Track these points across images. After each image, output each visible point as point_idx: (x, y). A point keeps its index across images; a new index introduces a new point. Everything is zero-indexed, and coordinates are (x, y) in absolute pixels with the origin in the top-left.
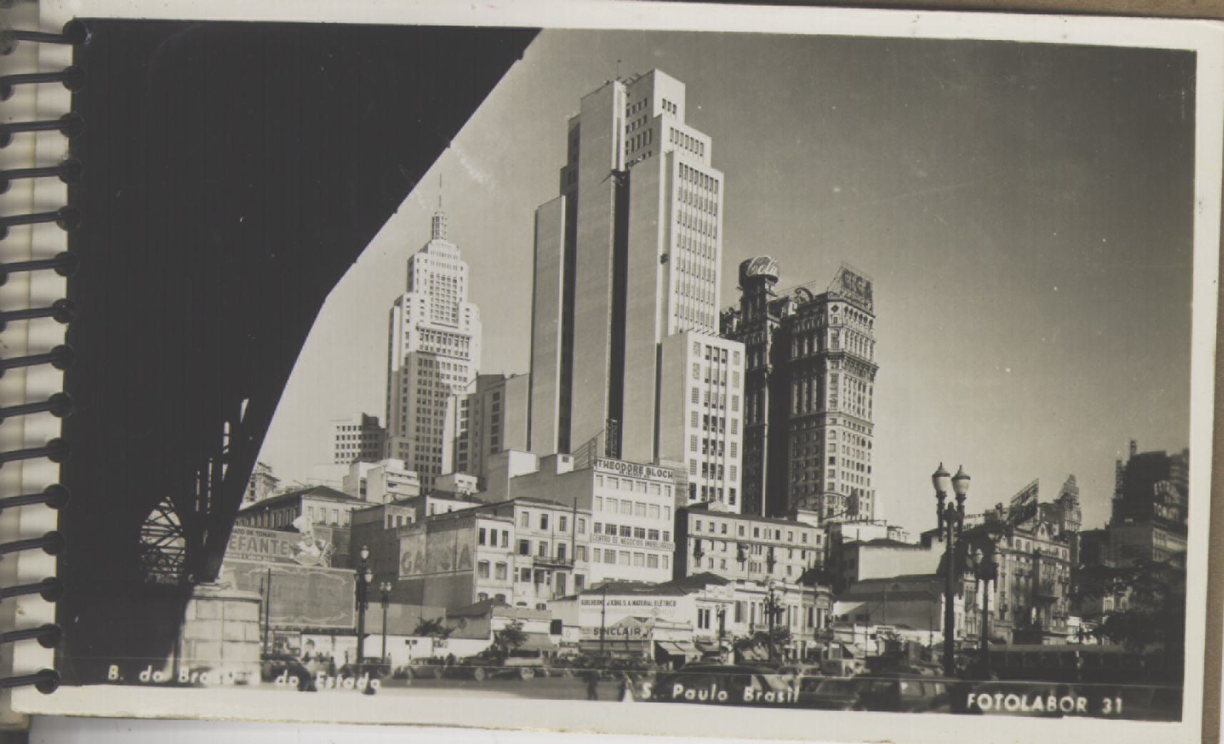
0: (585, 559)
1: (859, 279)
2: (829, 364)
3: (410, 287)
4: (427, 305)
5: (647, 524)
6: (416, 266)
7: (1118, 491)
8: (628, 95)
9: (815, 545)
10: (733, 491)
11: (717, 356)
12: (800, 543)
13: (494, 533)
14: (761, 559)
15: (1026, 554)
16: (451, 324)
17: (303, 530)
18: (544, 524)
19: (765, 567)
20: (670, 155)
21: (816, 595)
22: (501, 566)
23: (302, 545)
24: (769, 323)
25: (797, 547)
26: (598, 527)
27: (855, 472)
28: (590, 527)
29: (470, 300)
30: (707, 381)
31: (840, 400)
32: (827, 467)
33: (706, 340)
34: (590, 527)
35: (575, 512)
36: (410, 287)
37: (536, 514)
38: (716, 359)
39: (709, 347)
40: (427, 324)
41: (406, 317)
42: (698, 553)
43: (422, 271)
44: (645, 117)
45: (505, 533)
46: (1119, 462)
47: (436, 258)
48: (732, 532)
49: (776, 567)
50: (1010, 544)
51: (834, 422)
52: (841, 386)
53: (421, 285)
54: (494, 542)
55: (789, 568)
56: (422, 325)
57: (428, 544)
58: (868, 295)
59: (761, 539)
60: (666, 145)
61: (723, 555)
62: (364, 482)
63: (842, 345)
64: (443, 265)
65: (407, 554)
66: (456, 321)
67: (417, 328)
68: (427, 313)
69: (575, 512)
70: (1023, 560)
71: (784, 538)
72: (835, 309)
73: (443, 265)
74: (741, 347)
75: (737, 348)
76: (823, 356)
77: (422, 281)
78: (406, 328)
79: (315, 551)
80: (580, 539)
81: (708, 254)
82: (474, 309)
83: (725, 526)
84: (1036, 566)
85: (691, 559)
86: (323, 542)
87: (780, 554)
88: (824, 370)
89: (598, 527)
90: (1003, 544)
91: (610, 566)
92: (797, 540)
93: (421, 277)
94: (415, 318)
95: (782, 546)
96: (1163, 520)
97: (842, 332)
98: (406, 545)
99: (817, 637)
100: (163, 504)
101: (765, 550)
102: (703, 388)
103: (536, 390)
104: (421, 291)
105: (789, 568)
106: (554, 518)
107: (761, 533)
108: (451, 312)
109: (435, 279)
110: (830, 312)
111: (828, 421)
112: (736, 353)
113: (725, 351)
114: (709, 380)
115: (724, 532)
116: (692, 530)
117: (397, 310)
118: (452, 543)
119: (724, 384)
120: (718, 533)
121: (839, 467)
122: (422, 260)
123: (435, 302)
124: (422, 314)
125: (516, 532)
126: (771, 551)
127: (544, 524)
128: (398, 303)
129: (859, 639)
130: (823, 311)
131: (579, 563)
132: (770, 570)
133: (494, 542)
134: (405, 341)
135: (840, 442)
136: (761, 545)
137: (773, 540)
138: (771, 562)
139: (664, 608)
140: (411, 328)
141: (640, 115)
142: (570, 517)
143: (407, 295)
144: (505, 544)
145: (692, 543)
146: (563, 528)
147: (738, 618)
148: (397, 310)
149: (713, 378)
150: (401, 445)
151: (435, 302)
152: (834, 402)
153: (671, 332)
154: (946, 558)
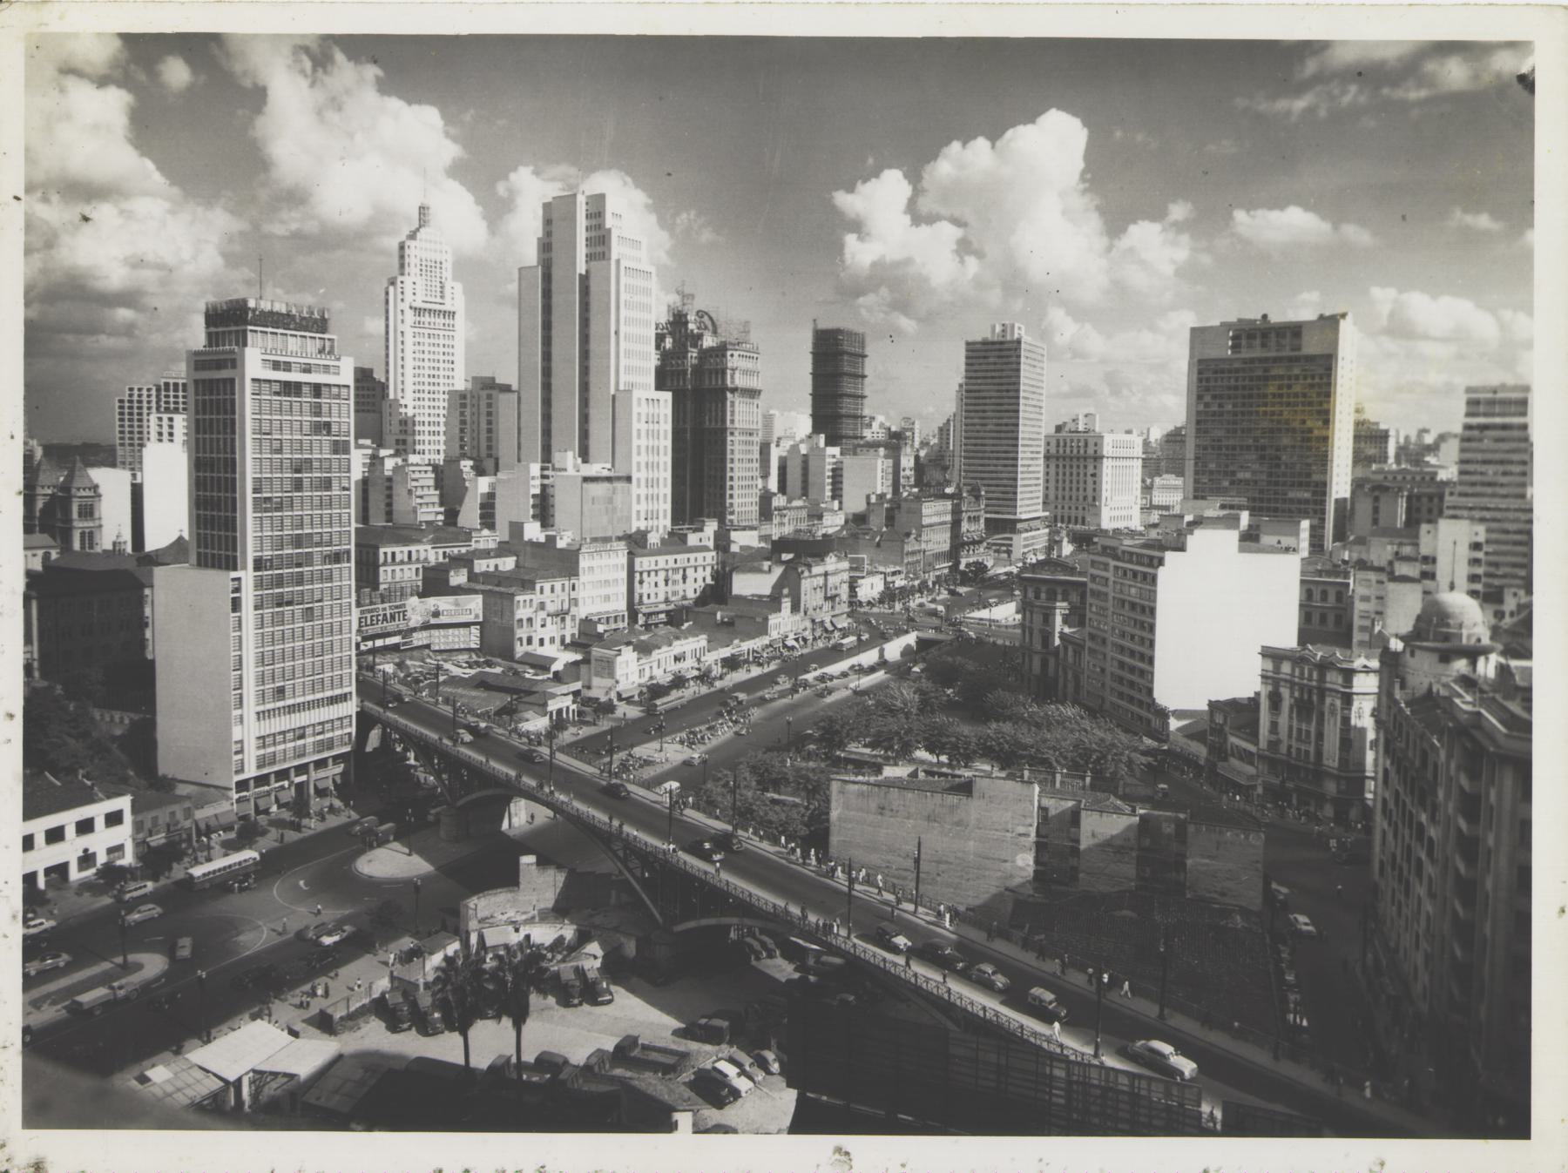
2: (729, 395)
6: (407, 251)
14: (679, 577)
18: (552, 590)
20: (618, 261)
22: (530, 620)
29: (455, 279)
32: (729, 483)
37: (547, 586)
40: (419, 304)
48: (662, 565)
53: (412, 269)
62: (390, 479)
71: (692, 563)
78: (401, 306)
81: (647, 292)
82: (459, 287)
87: (690, 572)
88: (725, 398)
90: (806, 574)
92: (700, 562)
94: (409, 297)
100: (782, 969)
102: (643, 427)
106: (558, 586)
114: (650, 420)
116: (637, 568)
117: (391, 289)
121: (736, 465)
125: (537, 598)
127: (552, 590)
128: (393, 282)
130: (724, 356)
134: (400, 317)
135: (737, 447)
140: (405, 306)
141: (594, 222)
143: (400, 278)
145: (637, 576)
148: (391, 289)
152: (732, 421)
153: (622, 387)
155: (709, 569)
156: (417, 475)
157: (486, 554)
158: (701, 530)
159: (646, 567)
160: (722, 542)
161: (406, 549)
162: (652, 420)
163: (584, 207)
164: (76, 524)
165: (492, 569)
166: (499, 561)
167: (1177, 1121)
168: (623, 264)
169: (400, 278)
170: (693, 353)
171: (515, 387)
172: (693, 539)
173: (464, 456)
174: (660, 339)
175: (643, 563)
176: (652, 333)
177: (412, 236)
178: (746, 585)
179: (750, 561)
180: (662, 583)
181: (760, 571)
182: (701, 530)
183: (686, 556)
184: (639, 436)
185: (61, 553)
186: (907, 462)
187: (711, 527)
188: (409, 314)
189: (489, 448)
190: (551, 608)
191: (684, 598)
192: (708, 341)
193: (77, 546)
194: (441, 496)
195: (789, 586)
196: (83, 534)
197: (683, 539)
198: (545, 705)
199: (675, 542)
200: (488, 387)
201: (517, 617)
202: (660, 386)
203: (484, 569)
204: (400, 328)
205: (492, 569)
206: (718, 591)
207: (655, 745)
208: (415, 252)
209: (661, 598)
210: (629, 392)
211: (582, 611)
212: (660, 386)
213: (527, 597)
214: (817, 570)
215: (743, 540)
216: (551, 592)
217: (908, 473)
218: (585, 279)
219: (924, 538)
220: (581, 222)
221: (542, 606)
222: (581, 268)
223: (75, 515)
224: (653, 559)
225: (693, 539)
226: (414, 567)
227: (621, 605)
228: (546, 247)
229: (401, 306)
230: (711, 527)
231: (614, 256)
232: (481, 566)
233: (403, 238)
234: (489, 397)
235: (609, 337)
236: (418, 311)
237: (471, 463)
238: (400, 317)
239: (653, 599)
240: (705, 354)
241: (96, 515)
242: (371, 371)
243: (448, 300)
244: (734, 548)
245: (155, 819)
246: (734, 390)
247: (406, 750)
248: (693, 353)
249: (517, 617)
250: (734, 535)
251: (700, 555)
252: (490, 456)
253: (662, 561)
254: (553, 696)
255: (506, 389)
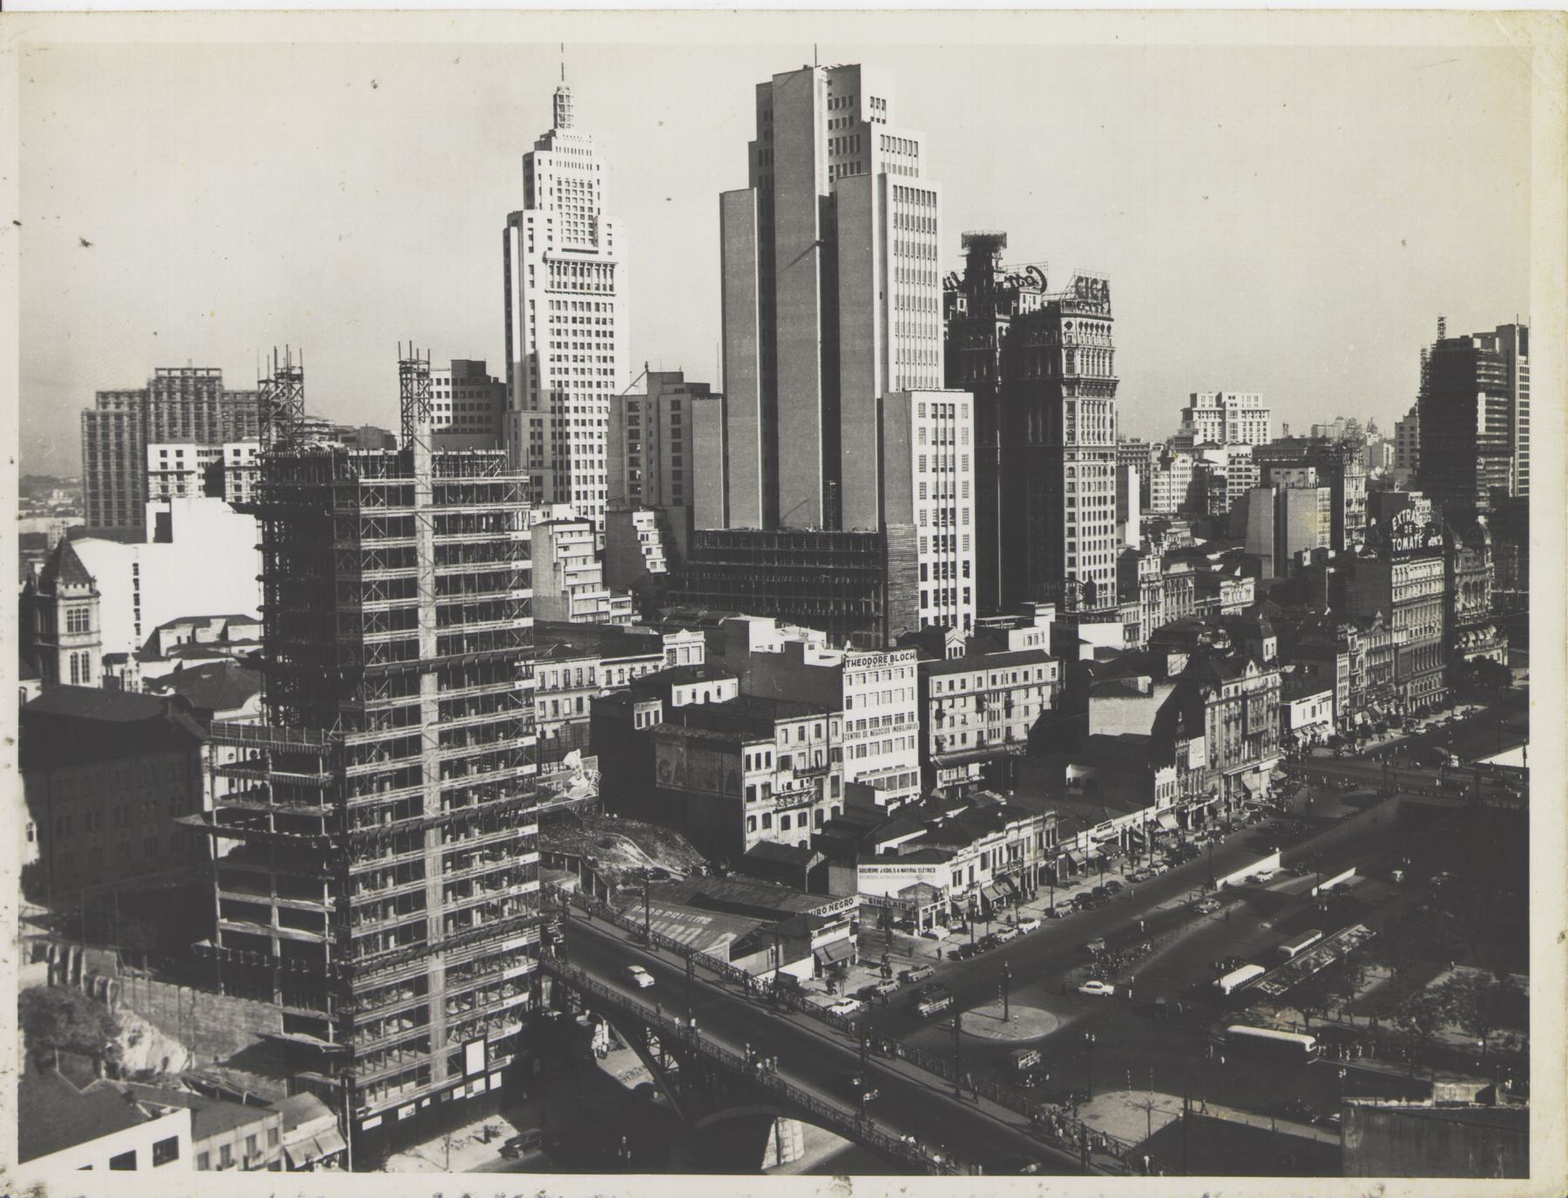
0: (840, 759)
1: (1095, 281)
2: (1064, 392)
3: (530, 204)
4: (555, 225)
5: (892, 710)
6: (537, 169)
7: (1423, 390)
8: (829, 83)
9: (1050, 679)
10: (966, 563)
11: (945, 412)
12: (1036, 681)
13: (758, 756)
14: (998, 706)
15: (1234, 699)
16: (590, 247)
17: (573, 765)
19: (1003, 713)
20: (883, 177)
21: (1044, 821)
23: (573, 780)
24: (998, 324)
25: (1033, 685)
26: (849, 725)
27: (1097, 508)
28: (842, 728)
30: (935, 443)
31: (1079, 431)
33: (930, 398)
34: (842, 728)
35: (828, 718)
36: (530, 204)
37: (793, 729)
38: (943, 416)
39: (935, 405)
40: (557, 254)
41: (527, 243)
42: (940, 715)
43: (545, 177)
44: (851, 118)
45: (768, 755)
46: (1424, 350)
47: (563, 157)
48: (971, 685)
49: (1014, 711)
50: (1219, 695)
51: (1072, 458)
52: (1079, 415)
53: (544, 198)
54: (758, 766)
55: (1027, 708)
56: (550, 255)
57: (689, 758)
58: (1106, 297)
59: (999, 686)
60: (877, 158)
61: (963, 710)
63: (1078, 370)
64: (574, 165)
65: (665, 763)
66: (594, 242)
67: (545, 260)
68: (556, 235)
69: (828, 718)
70: (1232, 705)
71: (1020, 680)
72: (1069, 325)
73: (574, 165)
74: (969, 398)
75: (964, 400)
76: (1058, 380)
77: (546, 191)
79: (584, 783)
80: (835, 741)
83: (963, 681)
84: (1244, 707)
85: (933, 722)
86: (590, 771)
87: (1017, 696)
89: (849, 725)
90: (1213, 698)
91: (862, 759)
92: (1033, 678)
93: (543, 184)
94: (541, 244)
95: (1019, 688)
96: (1404, 553)
97: (1078, 354)
98: (661, 753)
99: (1046, 857)
101: (1002, 696)
102: (930, 451)
103: (731, 421)
104: (546, 206)
105: (1027, 708)
106: (810, 728)
107: (998, 680)
108: (587, 229)
109: (564, 186)
110: (1064, 329)
111: (1066, 457)
112: (965, 406)
113: (953, 405)
115: (963, 687)
116: (934, 693)
118: (717, 765)
119: (952, 443)
120: (958, 689)
122: (545, 162)
123: (566, 218)
124: (550, 238)
125: (776, 750)
126: (1009, 696)
127: (802, 737)
129: (1082, 844)
131: (834, 766)
132: (1008, 715)
133: (758, 766)
136: (998, 691)
137: (1011, 684)
138: (1009, 706)
139: (926, 874)
140: (535, 259)
142: (823, 723)
143: (527, 214)
144: (768, 764)
145: (935, 705)
146: (818, 734)
147: (984, 866)
148: (514, 231)
149: (941, 438)
150: (532, 422)
151: (566, 218)
152: (1072, 436)
153: (893, 388)
154: (1164, 715)
155: (1047, 691)
156: (566, 540)
157: (688, 675)
158: (1031, 624)
159: (946, 690)
160: (1065, 640)
161: (560, 667)
162: (944, 440)
163: (825, 89)
164: (63, 641)
165: (700, 700)
166: (711, 686)
167: (920, 1167)
168: (893, 179)
169: (527, 214)
170: (1002, 324)
171: (716, 387)
172: (1018, 641)
173: (636, 505)
174: (949, 300)
175: (940, 684)
176: (938, 293)
177: (545, 143)
178: (1113, 717)
179: (1116, 673)
180: (973, 717)
181: (1133, 693)
182: (1031, 624)
183: (1010, 670)
184: (923, 469)
185: (43, 688)
186: (1354, 491)
187: (1045, 618)
188: (542, 271)
189: (677, 489)
190: (799, 763)
191: (1009, 739)
192: (1029, 303)
193: (65, 678)
194: (605, 572)
195: (1182, 718)
196: (74, 658)
197: (1002, 639)
198: (807, 938)
199: (987, 647)
200: (669, 385)
201: (748, 783)
202: (952, 382)
203: (687, 700)
204: (529, 294)
205: (700, 700)
206: (1062, 724)
207: (997, 1010)
208: (545, 165)
209: (972, 741)
210: (906, 395)
211: (850, 769)
212: (952, 382)
213: (762, 749)
214: (1230, 689)
215: (1099, 636)
216: (792, 739)
217: (1355, 508)
218: (829, 204)
219: (1396, 622)
220: (822, 114)
221: (785, 763)
222: (822, 187)
223: (62, 627)
224: (957, 678)
225: (1018, 641)
226: (574, 697)
227: (909, 759)
228: (762, 156)
229: (529, 259)
230: (1045, 618)
231: (876, 170)
232: (683, 695)
233: (531, 148)
234: (676, 405)
235: (871, 303)
236: (556, 266)
237: (651, 515)
238: (528, 277)
239: (959, 746)
240: (1019, 322)
241: (93, 627)
242: (483, 364)
243: (603, 246)
244: (1086, 653)
245: (226, 1149)
246: (1073, 383)
247: (594, 1020)
248: (1002, 324)
249: (748, 783)
250: (1085, 631)
251: (1032, 669)
252: (677, 502)
253: (970, 679)
254: (819, 923)
255: (701, 390)
